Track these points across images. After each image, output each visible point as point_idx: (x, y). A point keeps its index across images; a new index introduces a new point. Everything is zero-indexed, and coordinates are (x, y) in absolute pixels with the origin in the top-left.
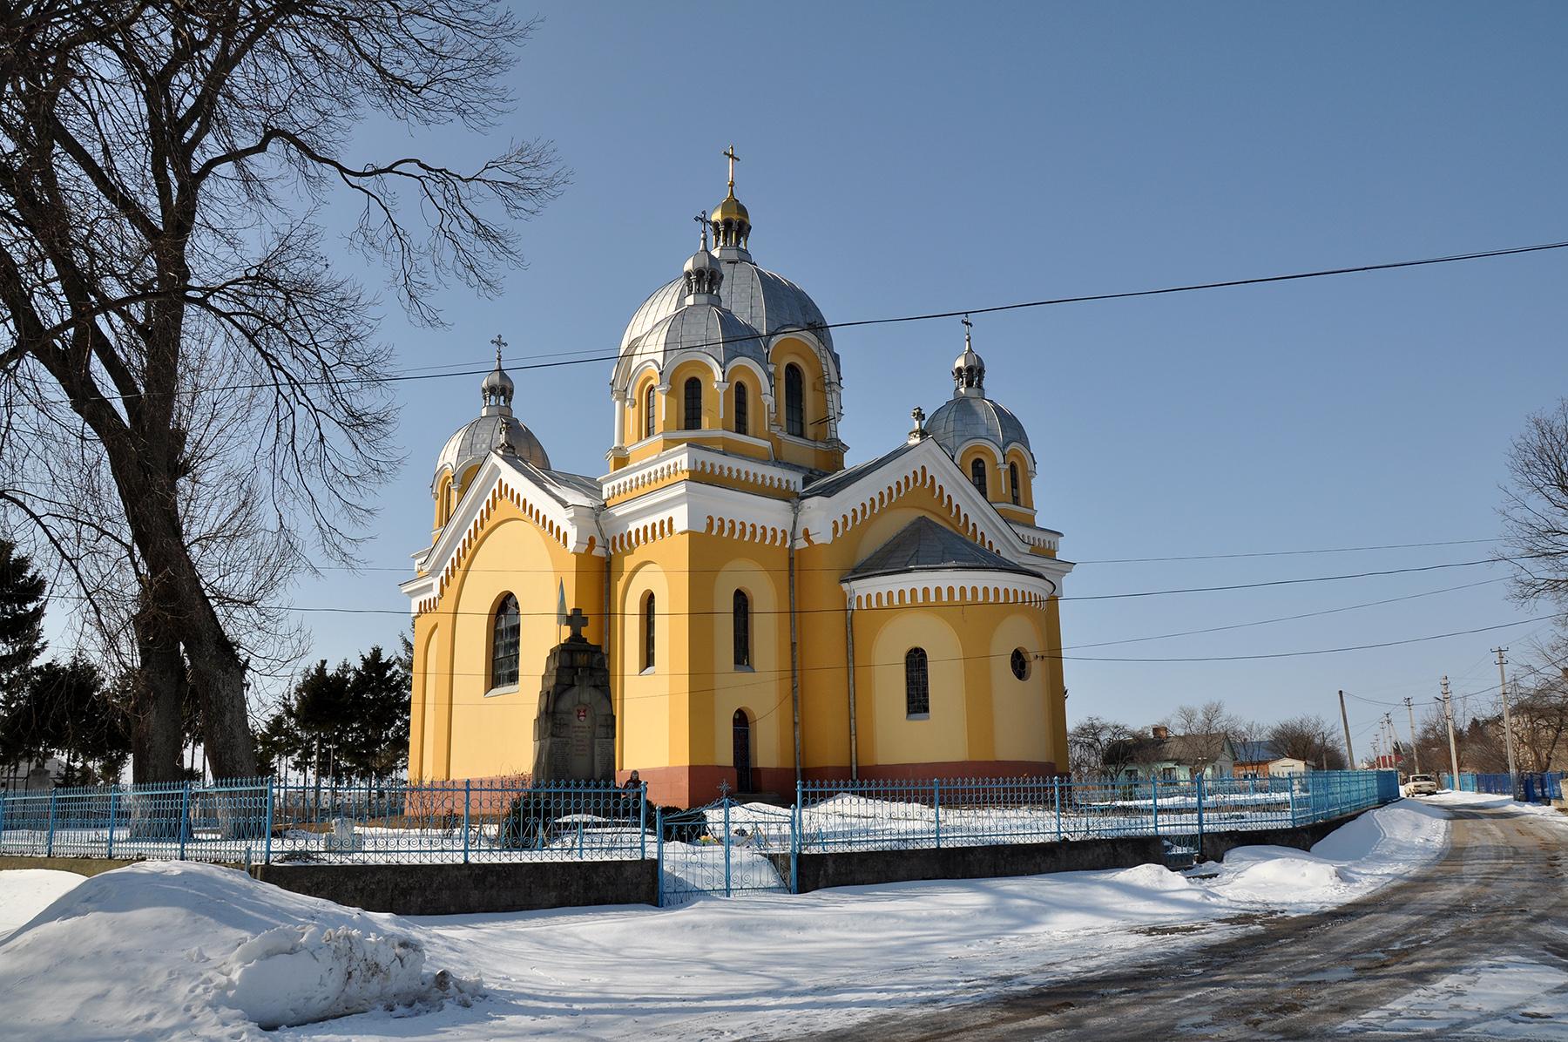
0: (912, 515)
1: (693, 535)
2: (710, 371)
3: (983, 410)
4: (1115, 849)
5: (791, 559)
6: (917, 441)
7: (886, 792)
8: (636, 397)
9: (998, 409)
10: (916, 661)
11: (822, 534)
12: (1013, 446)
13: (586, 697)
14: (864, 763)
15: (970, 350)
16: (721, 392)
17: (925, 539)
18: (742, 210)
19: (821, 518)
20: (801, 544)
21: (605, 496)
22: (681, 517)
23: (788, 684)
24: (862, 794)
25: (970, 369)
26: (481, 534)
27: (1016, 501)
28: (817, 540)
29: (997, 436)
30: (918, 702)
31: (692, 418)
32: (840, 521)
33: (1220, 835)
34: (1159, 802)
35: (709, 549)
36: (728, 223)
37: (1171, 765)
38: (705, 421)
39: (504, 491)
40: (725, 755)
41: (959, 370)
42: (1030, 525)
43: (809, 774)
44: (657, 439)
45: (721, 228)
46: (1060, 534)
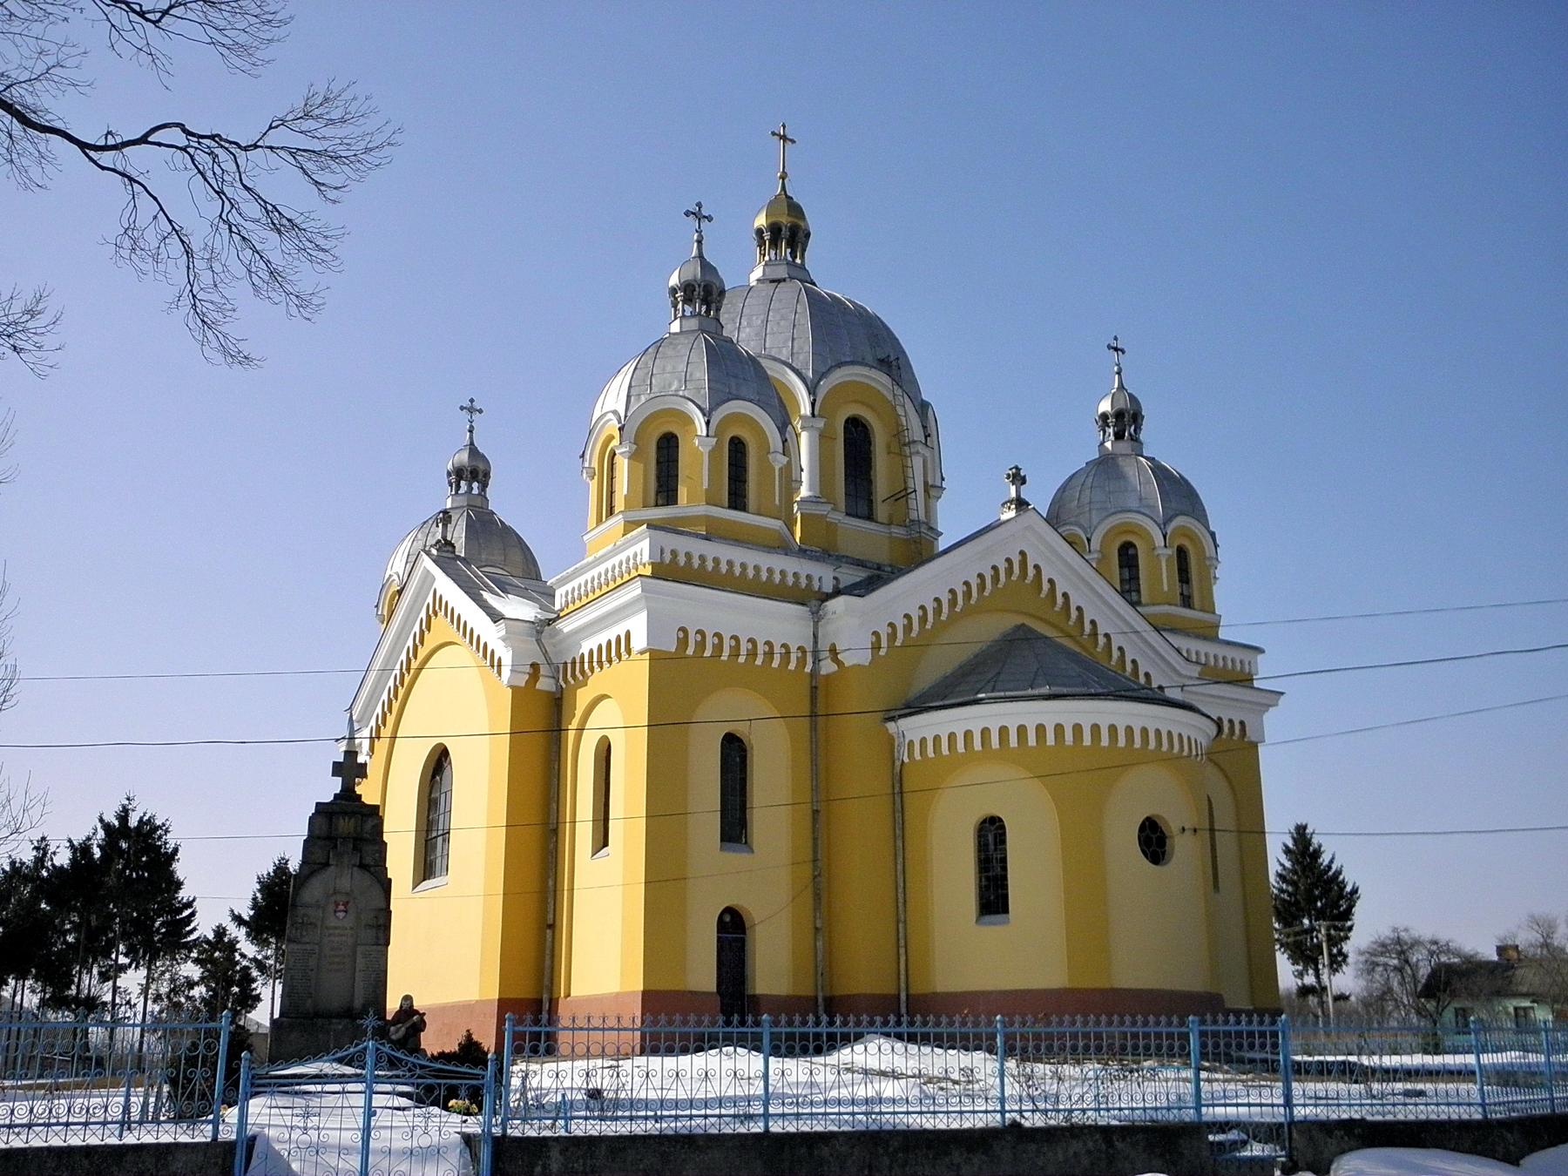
0: (1009, 622)
1: (657, 658)
2: (689, 421)
3: (1137, 474)
4: (1110, 1144)
5: (814, 689)
6: (1012, 514)
7: (951, 1037)
8: (595, 464)
9: (1160, 471)
10: (991, 837)
11: (856, 655)
12: (1180, 521)
13: (345, 883)
14: (918, 988)
15: (1121, 387)
16: (705, 450)
17: (1026, 652)
18: (795, 209)
19: (854, 626)
20: (828, 667)
21: (557, 607)
22: (638, 628)
23: (807, 871)
24: (912, 1039)
25: (1119, 415)
26: (414, 665)
27: (1187, 601)
28: (848, 659)
29: (1155, 507)
30: (994, 898)
31: (666, 490)
32: (884, 632)
33: (1326, 1127)
34: (1487, 1059)
35: (678, 675)
36: (775, 229)
37: (1527, 1004)
38: (683, 493)
39: (439, 606)
40: (703, 975)
41: (1104, 416)
42: (1208, 632)
43: (834, 1005)
44: (617, 521)
45: (767, 236)
46: (1261, 651)
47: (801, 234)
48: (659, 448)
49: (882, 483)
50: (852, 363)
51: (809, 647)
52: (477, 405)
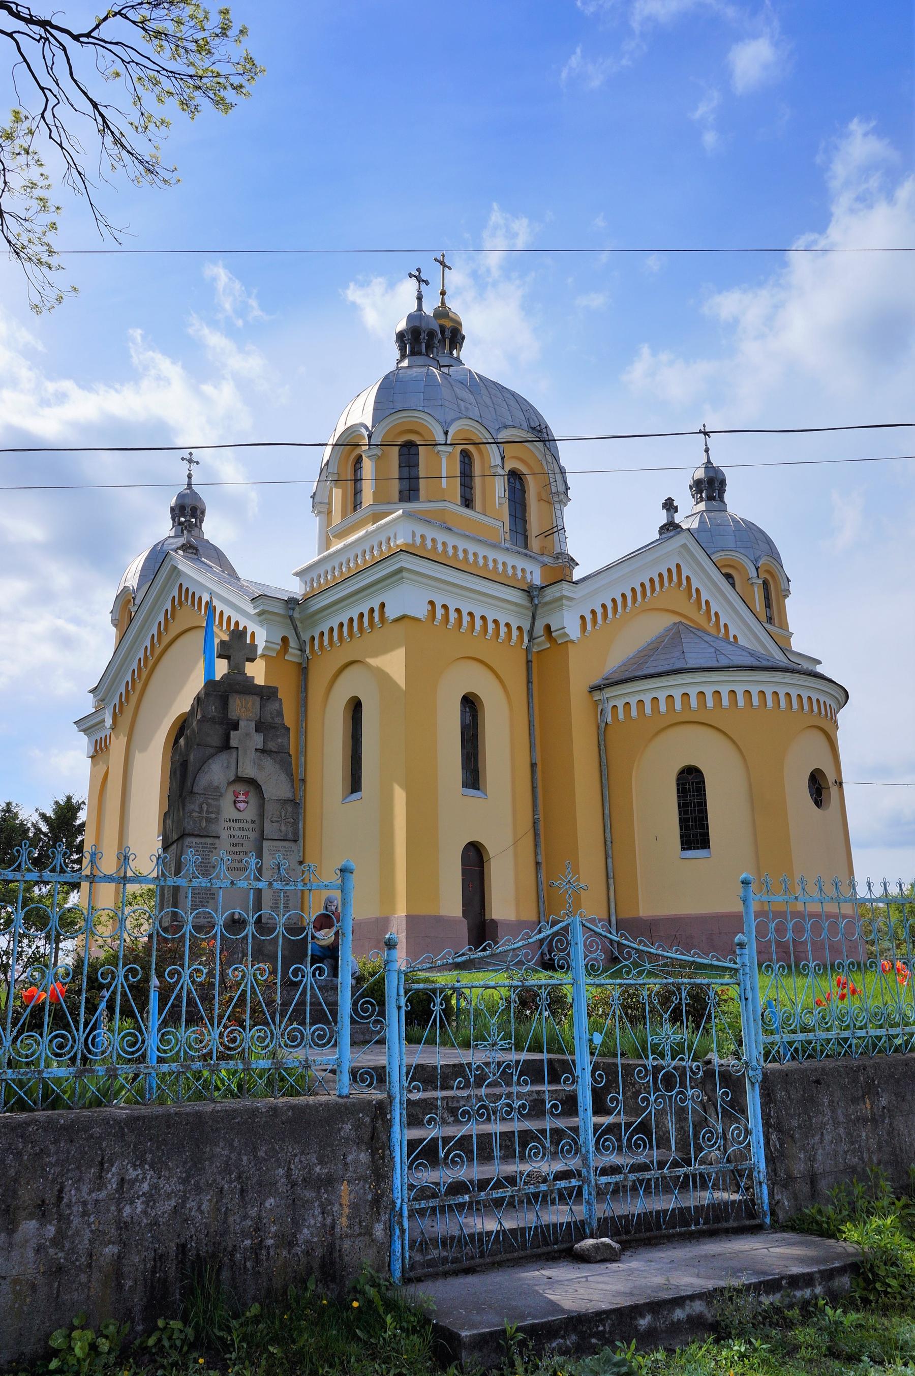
0: (668, 620)
10: (691, 784)
27: (770, 620)
30: (695, 832)
31: (409, 490)
40: (451, 904)
47: (459, 337)
49: (535, 526)
51: (526, 626)
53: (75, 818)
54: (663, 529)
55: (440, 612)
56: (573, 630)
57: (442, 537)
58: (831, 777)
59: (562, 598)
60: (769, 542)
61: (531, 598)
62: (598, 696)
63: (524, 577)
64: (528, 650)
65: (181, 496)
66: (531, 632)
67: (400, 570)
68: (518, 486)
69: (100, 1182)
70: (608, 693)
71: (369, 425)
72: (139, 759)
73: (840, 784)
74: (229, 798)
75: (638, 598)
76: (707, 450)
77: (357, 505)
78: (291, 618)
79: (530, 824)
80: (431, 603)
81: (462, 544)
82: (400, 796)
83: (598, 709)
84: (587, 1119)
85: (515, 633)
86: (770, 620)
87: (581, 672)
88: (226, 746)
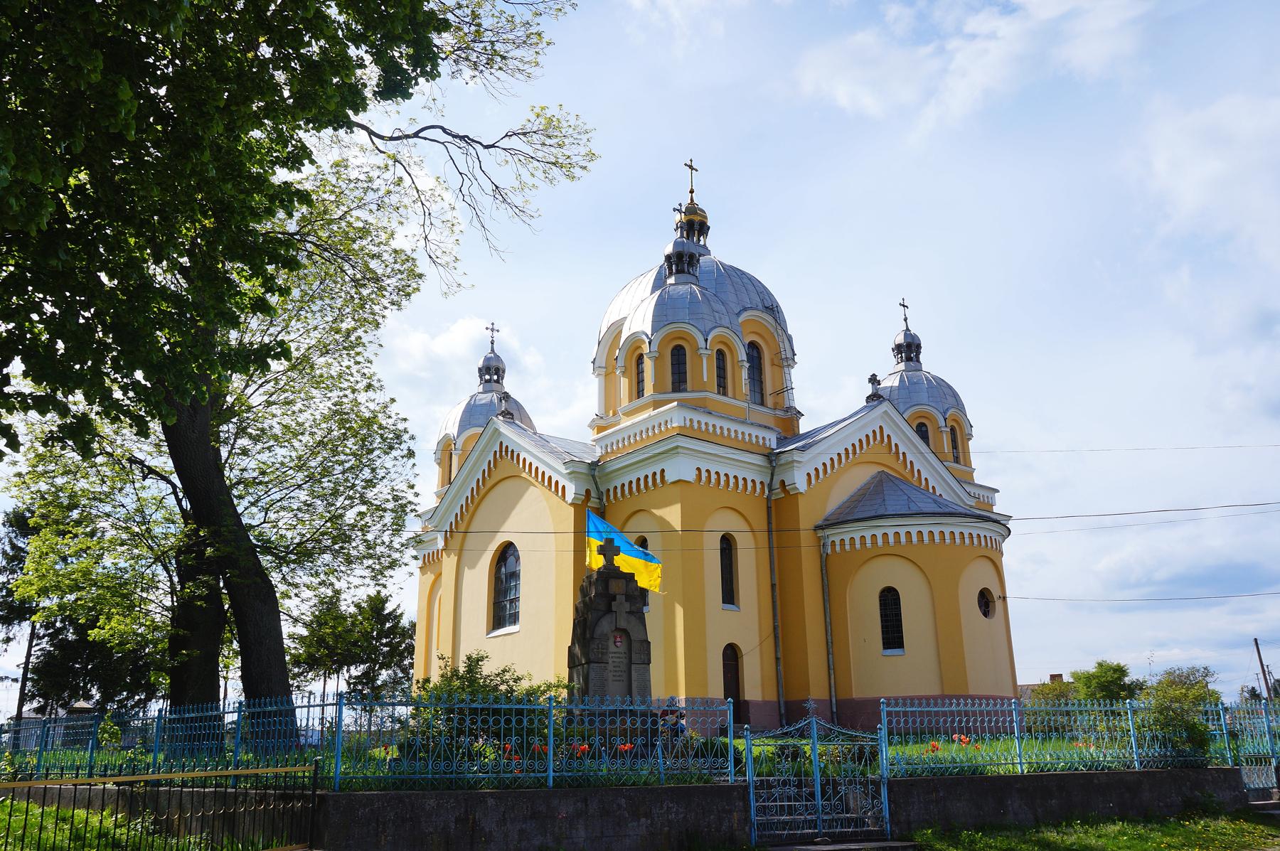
0: (874, 470)
10: (890, 600)
14: (842, 696)
27: (957, 460)
30: (893, 636)
31: (679, 381)
40: (716, 689)
46: (997, 491)
48: (672, 355)
49: (769, 387)
50: (751, 308)
51: (767, 481)
52: (496, 327)
53: (383, 609)
54: (869, 399)
55: (704, 475)
56: (801, 484)
57: (704, 419)
58: (996, 593)
59: (793, 461)
60: (955, 395)
61: (771, 462)
62: (820, 533)
63: (764, 444)
64: (768, 499)
65: (487, 359)
66: (770, 485)
67: (677, 447)
68: (755, 354)
69: (662, 808)
70: (828, 532)
71: (649, 333)
72: (468, 574)
73: (1004, 598)
74: (612, 640)
75: (851, 455)
76: (906, 320)
77: (640, 393)
78: (593, 476)
79: (771, 629)
80: (698, 469)
81: (719, 423)
82: (679, 611)
83: (821, 544)
84: (819, 802)
85: (758, 486)
86: (957, 460)
87: (808, 515)
88: (609, 610)
